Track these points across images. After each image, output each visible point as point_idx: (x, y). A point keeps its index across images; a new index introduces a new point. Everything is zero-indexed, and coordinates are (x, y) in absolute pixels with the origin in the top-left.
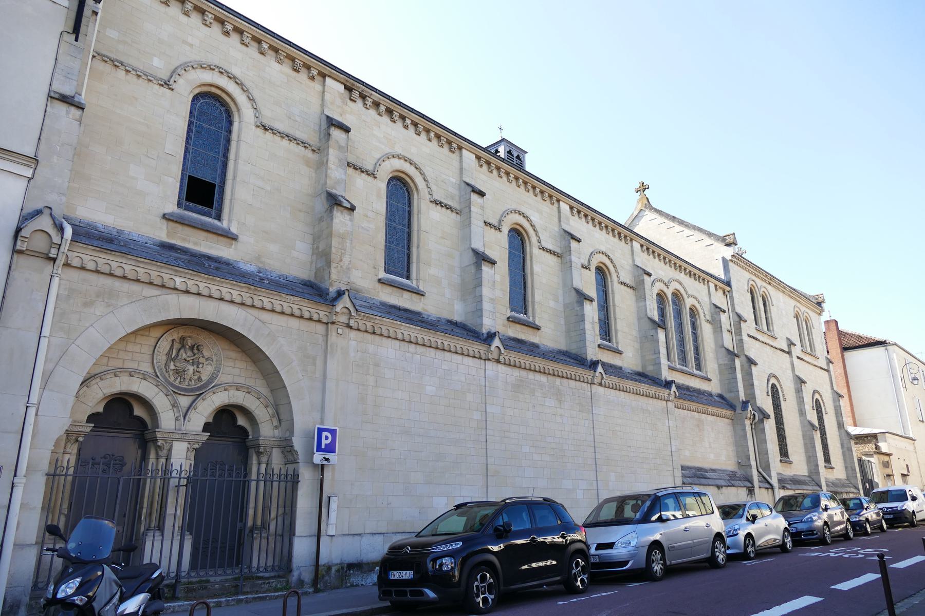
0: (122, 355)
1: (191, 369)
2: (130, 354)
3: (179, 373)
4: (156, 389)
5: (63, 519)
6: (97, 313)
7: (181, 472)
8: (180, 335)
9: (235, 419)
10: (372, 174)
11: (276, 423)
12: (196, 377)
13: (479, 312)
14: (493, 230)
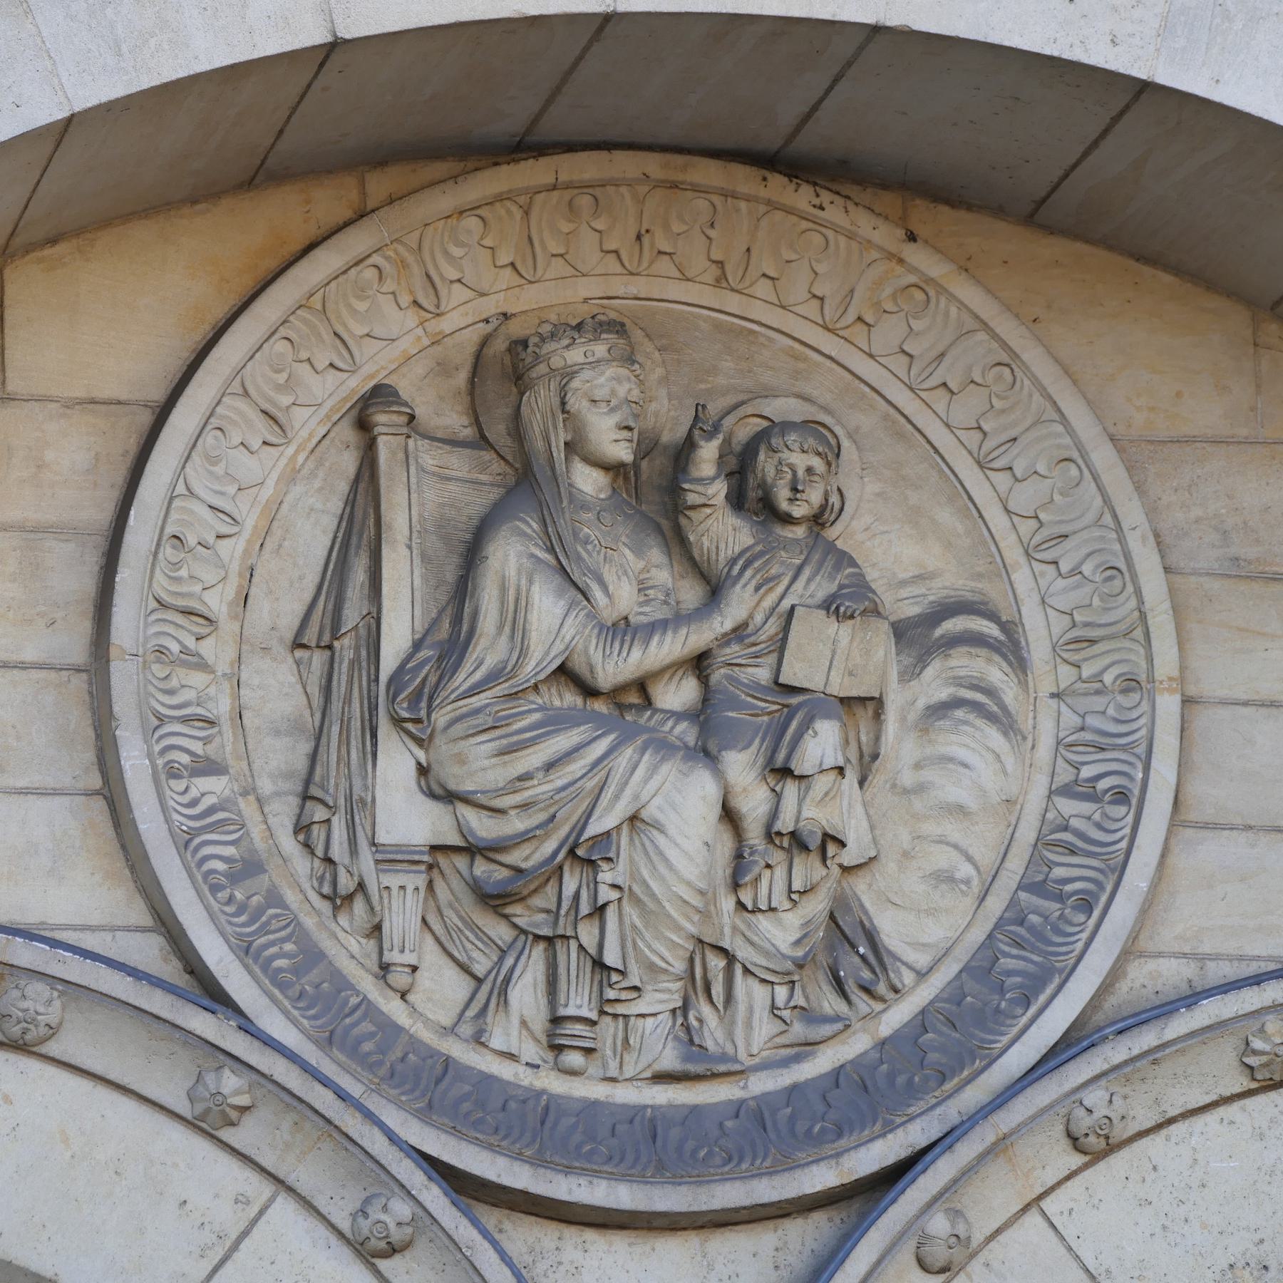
1: (680, 812)
3: (524, 889)
8: (462, 319)
12: (782, 933)
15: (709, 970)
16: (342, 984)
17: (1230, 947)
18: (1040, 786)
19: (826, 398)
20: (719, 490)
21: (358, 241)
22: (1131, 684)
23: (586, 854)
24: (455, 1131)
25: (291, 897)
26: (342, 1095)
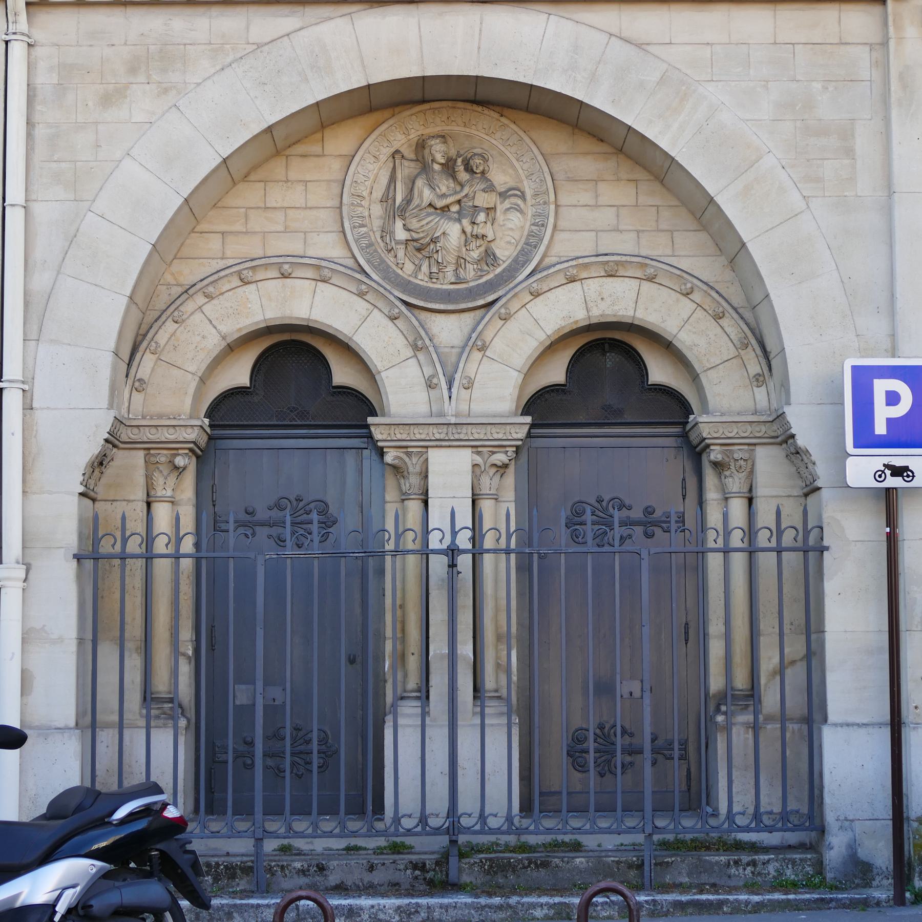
0: (257, 222)
1: (453, 232)
2: (280, 216)
3: (422, 247)
4: (361, 305)
5: (185, 669)
6: (139, 117)
7: (780, 533)
8: (414, 136)
9: (641, 368)
11: (755, 367)
12: (475, 254)
15: (461, 261)
16: (388, 267)
17: (566, 254)
18: (528, 224)
19: (486, 148)
20: (462, 168)
21: (391, 122)
22: (545, 203)
23: (434, 241)
24: (409, 295)
25: (380, 251)
26: (385, 289)
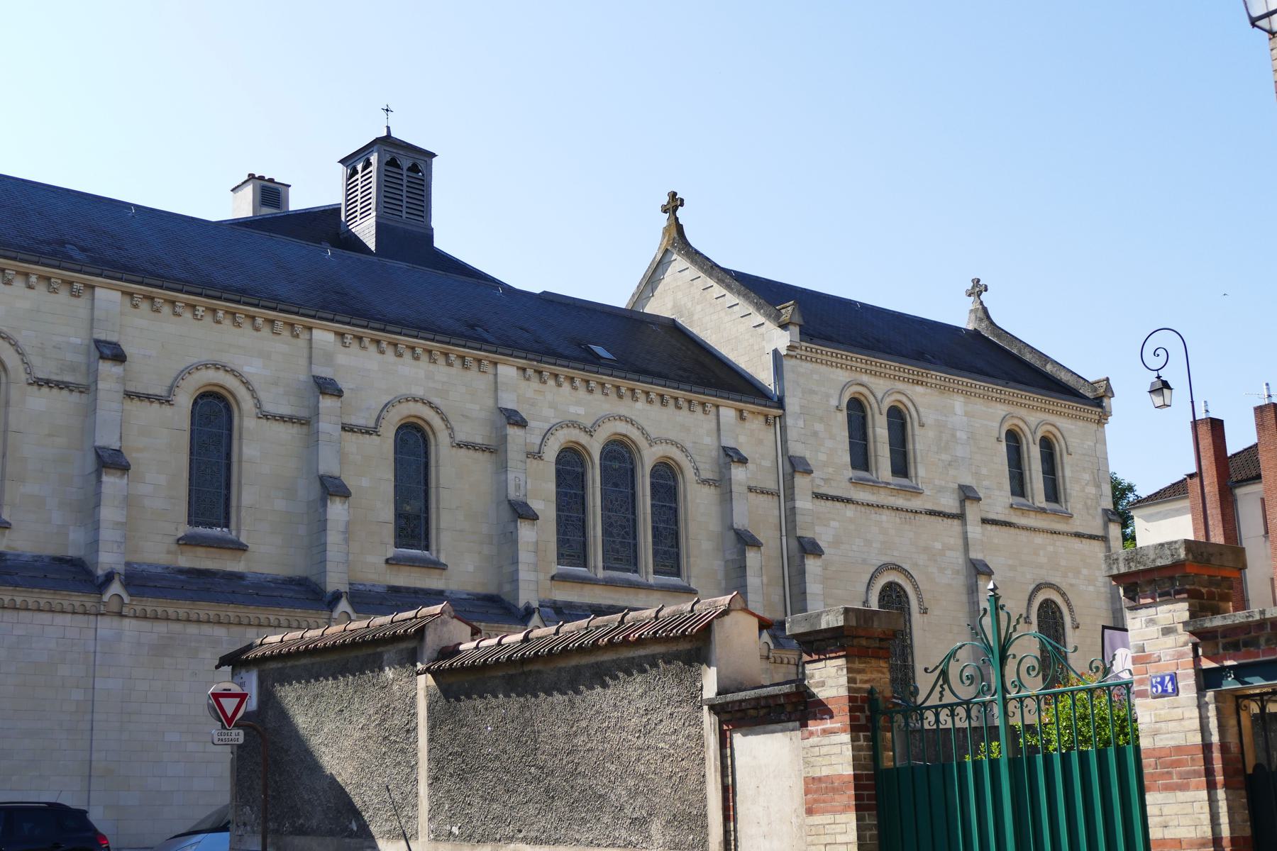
10: (165, 400)
13: (94, 544)
14: (156, 405)
